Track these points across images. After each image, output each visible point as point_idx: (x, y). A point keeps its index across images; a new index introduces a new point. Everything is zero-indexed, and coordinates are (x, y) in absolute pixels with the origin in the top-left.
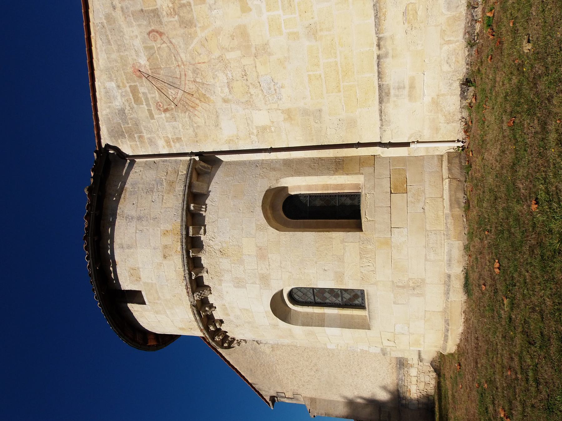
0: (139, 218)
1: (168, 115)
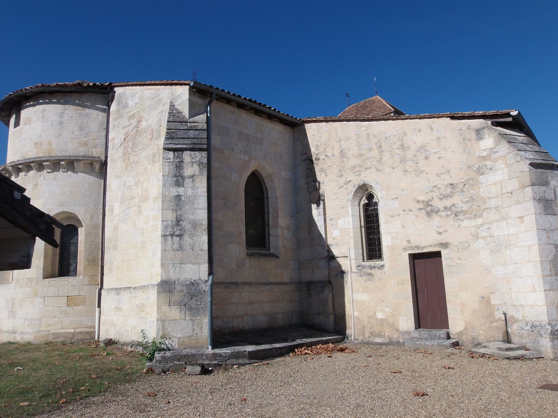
0: (61, 123)
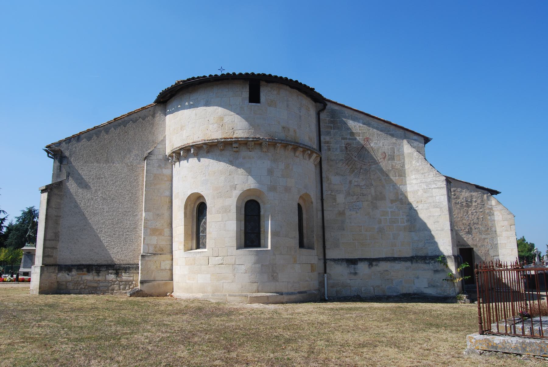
1: (344, 148)
